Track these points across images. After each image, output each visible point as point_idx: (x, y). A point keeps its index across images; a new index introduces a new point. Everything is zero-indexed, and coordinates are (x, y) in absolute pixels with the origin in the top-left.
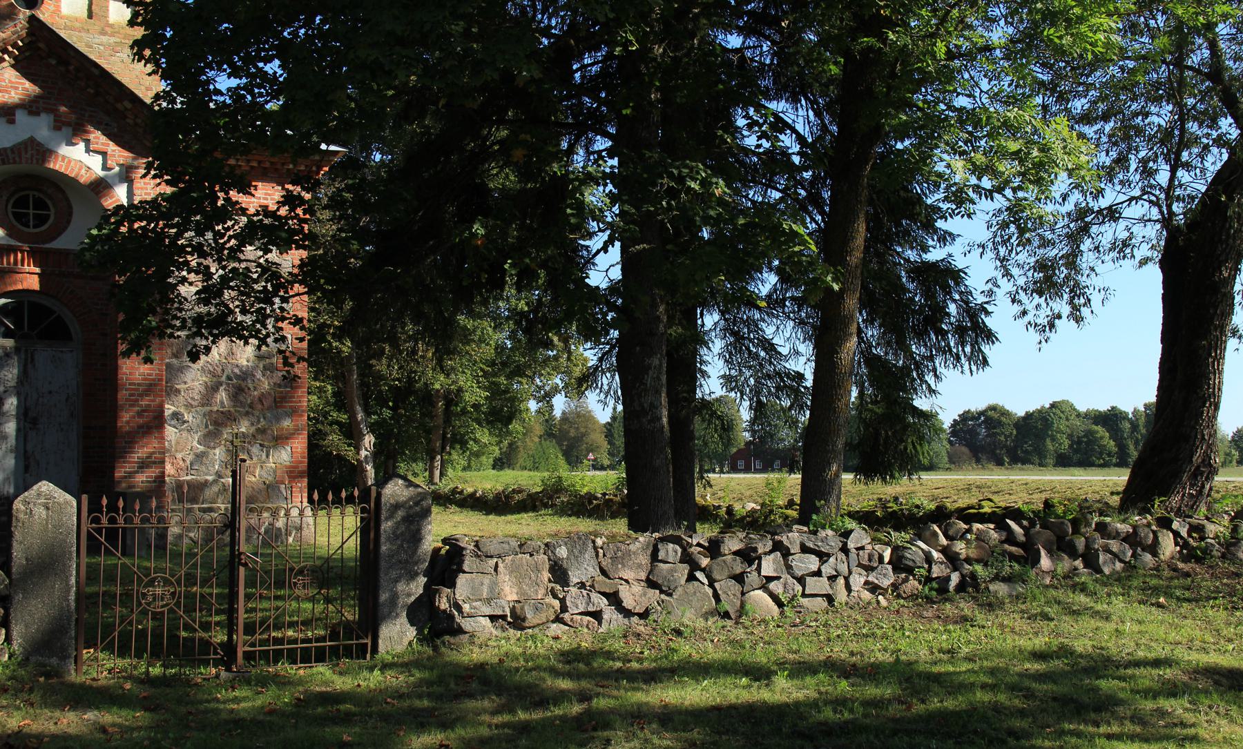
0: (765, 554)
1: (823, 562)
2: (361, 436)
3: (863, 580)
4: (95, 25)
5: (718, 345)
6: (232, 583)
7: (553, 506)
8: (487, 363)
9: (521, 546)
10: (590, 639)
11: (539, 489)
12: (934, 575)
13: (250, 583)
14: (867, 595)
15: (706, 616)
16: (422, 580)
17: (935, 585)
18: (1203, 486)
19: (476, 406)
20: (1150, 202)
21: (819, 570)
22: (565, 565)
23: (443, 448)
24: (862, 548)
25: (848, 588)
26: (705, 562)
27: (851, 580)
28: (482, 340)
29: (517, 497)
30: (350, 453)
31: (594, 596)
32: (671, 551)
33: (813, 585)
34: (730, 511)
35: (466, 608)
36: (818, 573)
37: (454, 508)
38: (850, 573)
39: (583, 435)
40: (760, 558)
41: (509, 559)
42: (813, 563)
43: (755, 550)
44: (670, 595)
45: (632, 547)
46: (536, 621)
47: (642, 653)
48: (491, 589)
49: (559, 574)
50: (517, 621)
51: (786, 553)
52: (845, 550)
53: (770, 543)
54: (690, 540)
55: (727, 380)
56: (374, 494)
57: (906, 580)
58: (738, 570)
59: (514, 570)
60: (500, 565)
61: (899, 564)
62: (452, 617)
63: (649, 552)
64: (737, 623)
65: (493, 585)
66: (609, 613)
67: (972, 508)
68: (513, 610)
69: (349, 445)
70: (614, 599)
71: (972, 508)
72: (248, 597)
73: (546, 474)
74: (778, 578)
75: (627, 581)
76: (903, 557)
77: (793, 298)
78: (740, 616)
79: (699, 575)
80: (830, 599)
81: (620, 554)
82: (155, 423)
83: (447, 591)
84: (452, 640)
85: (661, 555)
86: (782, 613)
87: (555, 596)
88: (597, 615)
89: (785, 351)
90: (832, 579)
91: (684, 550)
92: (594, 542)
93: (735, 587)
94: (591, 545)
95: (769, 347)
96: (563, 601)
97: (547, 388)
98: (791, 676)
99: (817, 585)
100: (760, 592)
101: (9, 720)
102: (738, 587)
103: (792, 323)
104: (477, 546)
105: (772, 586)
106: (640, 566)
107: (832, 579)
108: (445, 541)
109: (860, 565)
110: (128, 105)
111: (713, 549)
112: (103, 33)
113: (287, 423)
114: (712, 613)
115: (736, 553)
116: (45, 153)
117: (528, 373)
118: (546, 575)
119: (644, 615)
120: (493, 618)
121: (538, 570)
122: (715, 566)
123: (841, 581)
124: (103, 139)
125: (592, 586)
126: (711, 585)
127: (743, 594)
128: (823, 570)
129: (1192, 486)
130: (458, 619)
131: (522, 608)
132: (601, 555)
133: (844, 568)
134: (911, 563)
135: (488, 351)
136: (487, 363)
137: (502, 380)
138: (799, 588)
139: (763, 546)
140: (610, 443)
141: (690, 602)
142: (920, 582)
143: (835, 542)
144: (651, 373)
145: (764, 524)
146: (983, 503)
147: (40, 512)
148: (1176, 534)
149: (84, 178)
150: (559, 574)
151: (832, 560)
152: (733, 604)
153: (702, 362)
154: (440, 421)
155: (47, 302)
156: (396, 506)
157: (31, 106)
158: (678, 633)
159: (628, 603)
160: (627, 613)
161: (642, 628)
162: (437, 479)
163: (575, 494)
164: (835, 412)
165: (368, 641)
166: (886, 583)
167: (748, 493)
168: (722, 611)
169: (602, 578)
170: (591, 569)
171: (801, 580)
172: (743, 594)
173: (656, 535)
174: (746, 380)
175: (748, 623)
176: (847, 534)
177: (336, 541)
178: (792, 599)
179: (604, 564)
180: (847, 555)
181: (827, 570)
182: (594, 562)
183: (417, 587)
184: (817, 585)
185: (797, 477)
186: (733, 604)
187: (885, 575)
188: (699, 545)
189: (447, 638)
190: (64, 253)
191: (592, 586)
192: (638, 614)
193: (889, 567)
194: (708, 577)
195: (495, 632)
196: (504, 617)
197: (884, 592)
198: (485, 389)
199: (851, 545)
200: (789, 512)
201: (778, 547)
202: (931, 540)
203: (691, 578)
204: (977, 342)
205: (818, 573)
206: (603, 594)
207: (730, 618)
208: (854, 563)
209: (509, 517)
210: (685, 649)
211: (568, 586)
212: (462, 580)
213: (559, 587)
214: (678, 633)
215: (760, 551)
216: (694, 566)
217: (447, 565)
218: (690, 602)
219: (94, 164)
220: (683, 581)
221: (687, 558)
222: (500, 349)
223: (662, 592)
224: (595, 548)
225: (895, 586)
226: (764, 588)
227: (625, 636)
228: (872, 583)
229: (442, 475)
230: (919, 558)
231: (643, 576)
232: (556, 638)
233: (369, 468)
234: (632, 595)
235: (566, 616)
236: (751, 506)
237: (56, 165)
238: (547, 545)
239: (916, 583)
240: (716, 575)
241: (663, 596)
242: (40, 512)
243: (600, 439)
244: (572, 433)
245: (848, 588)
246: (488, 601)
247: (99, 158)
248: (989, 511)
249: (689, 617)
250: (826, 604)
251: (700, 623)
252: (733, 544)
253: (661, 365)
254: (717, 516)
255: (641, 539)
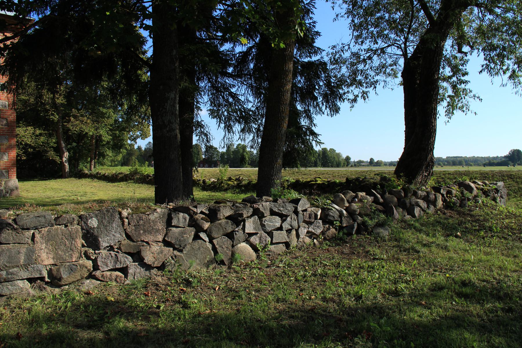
0: (248, 217)
1: (283, 221)
2: (64, 153)
3: (306, 231)
7: (133, 179)
8: (111, 125)
10: (116, 291)
11: (128, 173)
12: (345, 225)
14: (308, 240)
17: (345, 231)
18: (430, 172)
19: (108, 143)
20: (398, 47)
21: (281, 226)
22: (96, 233)
24: (306, 210)
25: (298, 236)
26: (206, 225)
27: (300, 231)
28: (108, 117)
29: (120, 176)
30: (57, 159)
31: (120, 255)
34: (204, 181)
36: (280, 229)
37: (96, 180)
38: (299, 227)
40: (244, 221)
41: (45, 230)
42: (277, 221)
43: (241, 215)
44: (181, 251)
45: (152, 217)
46: (71, 280)
47: (158, 307)
49: (91, 240)
50: (55, 280)
51: (261, 216)
52: (296, 212)
54: (195, 210)
57: (329, 229)
58: (230, 230)
59: (49, 239)
60: (37, 236)
61: (326, 219)
63: (165, 220)
64: (229, 268)
66: (134, 268)
67: (313, 181)
68: (50, 273)
69: (57, 156)
70: (137, 257)
71: (313, 181)
73: (130, 167)
74: (256, 234)
75: (147, 243)
76: (328, 215)
78: (231, 263)
79: (203, 235)
80: (287, 245)
81: (141, 222)
86: (258, 257)
87: (88, 258)
88: (124, 270)
90: (289, 231)
91: (191, 217)
92: (120, 213)
94: (118, 216)
95: (234, 96)
96: (95, 261)
97: (135, 136)
99: (280, 236)
100: (244, 244)
101: (46, 260)
102: (230, 242)
103: (246, 87)
105: (252, 239)
107: (289, 231)
109: (305, 222)
114: (211, 262)
115: (228, 218)
117: (128, 130)
118: (80, 241)
119: (162, 268)
121: (72, 237)
122: (214, 228)
123: (294, 232)
125: (119, 248)
126: (211, 242)
127: (233, 246)
128: (284, 226)
129: (426, 171)
131: (58, 270)
132: (126, 223)
133: (295, 224)
134: (332, 219)
135: (111, 121)
136: (111, 125)
137: (117, 132)
138: (269, 239)
142: (336, 229)
144: (169, 102)
145: (219, 187)
146: (317, 179)
148: (443, 195)
150: (91, 240)
152: (226, 254)
153: (198, 102)
154: (94, 147)
158: (188, 283)
159: (149, 259)
160: (148, 267)
161: (160, 279)
163: (142, 175)
164: (280, 127)
166: (319, 231)
167: (208, 174)
169: (127, 241)
170: (118, 235)
171: (270, 234)
172: (233, 246)
173: (171, 205)
174: (223, 112)
175: (238, 269)
176: (296, 202)
178: (265, 247)
179: (129, 230)
180: (297, 216)
181: (286, 226)
184: (280, 236)
187: (318, 227)
188: (202, 213)
191: (119, 248)
192: (157, 267)
193: (320, 221)
194: (208, 236)
195: (32, 292)
197: (317, 237)
198: (111, 135)
199: (300, 209)
200: (230, 182)
202: (340, 202)
203: (197, 237)
204: (334, 102)
205: (280, 229)
206: (129, 254)
207: (224, 264)
208: (301, 220)
209: (116, 184)
211: (99, 249)
213: (91, 251)
215: (245, 216)
216: (199, 229)
220: (190, 240)
221: (193, 223)
222: (116, 121)
223: (175, 249)
224: (121, 218)
225: (323, 233)
226: (247, 241)
227: (146, 287)
228: (311, 232)
230: (337, 215)
231: (160, 238)
235: (98, 273)
238: (80, 217)
239: (334, 230)
240: (214, 235)
241: (176, 252)
245: (298, 236)
246: (26, 266)
248: (321, 182)
253: (175, 98)
254: (199, 184)
255: (159, 210)
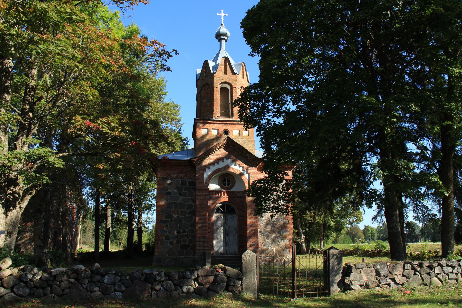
1: (453, 269)
4: (240, 137)
5: (411, 207)
6: (293, 276)
9: (367, 265)
11: (353, 249)
13: (298, 276)
15: (420, 285)
16: (341, 275)
23: (323, 238)
26: (418, 269)
31: (388, 279)
32: (408, 266)
33: (451, 276)
35: (353, 283)
36: (452, 272)
39: (357, 233)
40: (434, 268)
42: (450, 269)
43: (433, 266)
44: (409, 279)
48: (360, 278)
50: (367, 286)
51: (442, 266)
53: (437, 264)
55: (415, 218)
56: (327, 252)
59: (366, 272)
62: (350, 285)
65: (360, 276)
66: (392, 284)
68: (366, 283)
70: (393, 280)
72: (297, 280)
74: (440, 274)
77: (431, 193)
79: (417, 273)
80: (457, 280)
82: (255, 234)
83: (348, 278)
84: (350, 291)
85: (406, 268)
86: (442, 284)
87: (377, 279)
88: (389, 285)
89: (430, 208)
93: (428, 277)
95: (426, 207)
96: (379, 281)
98: (453, 304)
100: (435, 278)
102: (429, 276)
104: (355, 265)
106: (400, 271)
108: (346, 264)
110: (248, 155)
111: (421, 265)
112: (242, 138)
113: (287, 233)
115: (427, 267)
116: (228, 167)
118: (374, 274)
119: (402, 285)
120: (361, 285)
124: (243, 163)
126: (421, 276)
127: (430, 278)
130: (351, 286)
138: (447, 277)
139: (435, 264)
140: (364, 235)
141: (415, 281)
143: (456, 264)
147: (248, 257)
149: (238, 173)
151: (456, 268)
152: (428, 282)
154: (322, 231)
155: (230, 204)
156: (333, 255)
157: (227, 157)
158: (413, 290)
159: (397, 281)
160: (397, 284)
162: (322, 247)
165: (327, 291)
168: (425, 283)
171: (447, 274)
172: (430, 278)
175: (433, 287)
177: (318, 264)
181: (455, 271)
182: (387, 269)
183: (339, 278)
185: (440, 243)
186: (428, 282)
189: (348, 291)
190: (234, 192)
196: (363, 285)
200: (430, 254)
201: (439, 265)
203: (415, 274)
205: (452, 272)
210: (417, 295)
212: (352, 275)
214: (413, 290)
216: (415, 270)
217: (348, 271)
218: (415, 281)
219: (241, 170)
221: (413, 268)
223: (407, 278)
224: (387, 266)
226: (436, 277)
229: (323, 246)
232: (378, 291)
233: (304, 244)
234: (399, 279)
235: (381, 285)
236: (417, 253)
237: (230, 170)
238: (374, 265)
240: (422, 273)
242: (248, 257)
243: (361, 234)
244: (353, 233)
246: (359, 281)
247: (242, 168)
249: (415, 285)
250: (455, 282)
251: (419, 287)
252: (426, 264)
